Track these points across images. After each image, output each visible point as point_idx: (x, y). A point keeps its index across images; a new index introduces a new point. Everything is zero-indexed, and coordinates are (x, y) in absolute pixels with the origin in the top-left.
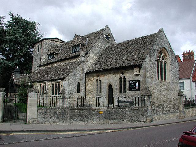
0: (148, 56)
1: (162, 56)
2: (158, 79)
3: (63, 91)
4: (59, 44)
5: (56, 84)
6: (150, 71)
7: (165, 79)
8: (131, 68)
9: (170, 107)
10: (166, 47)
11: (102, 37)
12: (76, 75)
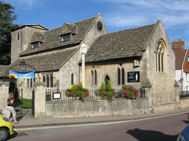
0: (148, 48)
1: (160, 47)
2: (157, 71)
3: (58, 84)
4: (41, 31)
5: (48, 76)
6: (150, 62)
7: (162, 71)
8: (130, 60)
9: (167, 98)
10: (164, 39)
11: (94, 26)
12: (70, 67)
